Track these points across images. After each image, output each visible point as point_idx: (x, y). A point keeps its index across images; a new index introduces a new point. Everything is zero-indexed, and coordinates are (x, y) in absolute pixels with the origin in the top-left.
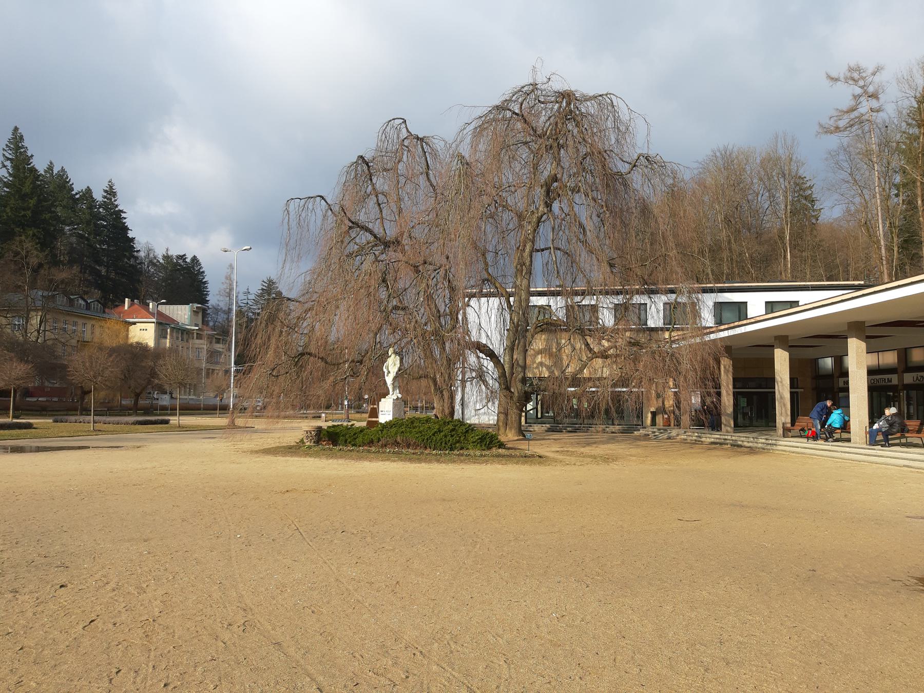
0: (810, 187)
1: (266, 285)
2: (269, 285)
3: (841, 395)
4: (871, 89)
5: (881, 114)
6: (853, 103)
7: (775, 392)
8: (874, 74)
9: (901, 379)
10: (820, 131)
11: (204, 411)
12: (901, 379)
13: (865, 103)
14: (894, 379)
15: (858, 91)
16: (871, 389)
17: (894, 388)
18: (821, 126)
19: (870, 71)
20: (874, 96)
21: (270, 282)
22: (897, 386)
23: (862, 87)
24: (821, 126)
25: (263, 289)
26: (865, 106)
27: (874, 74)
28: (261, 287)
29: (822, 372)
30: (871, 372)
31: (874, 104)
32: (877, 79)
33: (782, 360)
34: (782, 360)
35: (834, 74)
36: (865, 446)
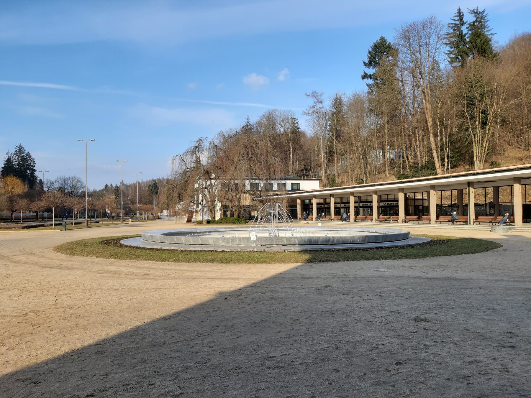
0: (297, 123)
1: (18, 148)
2: (20, 149)
3: (310, 210)
4: (320, 100)
5: (323, 109)
6: (314, 104)
7: (398, 206)
8: (321, 95)
9: (324, 206)
10: (303, 113)
11: (48, 220)
12: (324, 206)
13: (318, 105)
14: (323, 206)
15: (316, 100)
16: (317, 209)
17: (323, 208)
18: (304, 112)
19: (319, 94)
20: (321, 102)
21: (20, 147)
22: (360, 203)
23: (317, 99)
24: (304, 112)
25: (16, 151)
26: (318, 106)
27: (321, 95)
28: (14, 150)
29: (305, 204)
30: (317, 204)
31: (321, 105)
32: (322, 97)
33: (299, 201)
34: (299, 201)
35: (308, 94)
36: (322, 189)
